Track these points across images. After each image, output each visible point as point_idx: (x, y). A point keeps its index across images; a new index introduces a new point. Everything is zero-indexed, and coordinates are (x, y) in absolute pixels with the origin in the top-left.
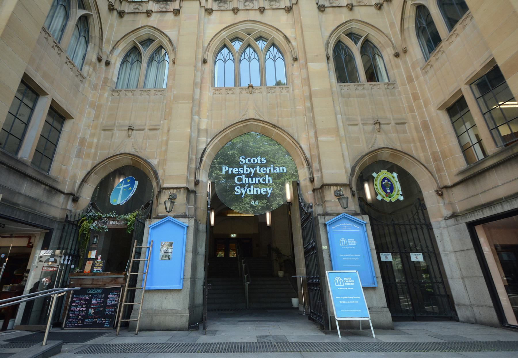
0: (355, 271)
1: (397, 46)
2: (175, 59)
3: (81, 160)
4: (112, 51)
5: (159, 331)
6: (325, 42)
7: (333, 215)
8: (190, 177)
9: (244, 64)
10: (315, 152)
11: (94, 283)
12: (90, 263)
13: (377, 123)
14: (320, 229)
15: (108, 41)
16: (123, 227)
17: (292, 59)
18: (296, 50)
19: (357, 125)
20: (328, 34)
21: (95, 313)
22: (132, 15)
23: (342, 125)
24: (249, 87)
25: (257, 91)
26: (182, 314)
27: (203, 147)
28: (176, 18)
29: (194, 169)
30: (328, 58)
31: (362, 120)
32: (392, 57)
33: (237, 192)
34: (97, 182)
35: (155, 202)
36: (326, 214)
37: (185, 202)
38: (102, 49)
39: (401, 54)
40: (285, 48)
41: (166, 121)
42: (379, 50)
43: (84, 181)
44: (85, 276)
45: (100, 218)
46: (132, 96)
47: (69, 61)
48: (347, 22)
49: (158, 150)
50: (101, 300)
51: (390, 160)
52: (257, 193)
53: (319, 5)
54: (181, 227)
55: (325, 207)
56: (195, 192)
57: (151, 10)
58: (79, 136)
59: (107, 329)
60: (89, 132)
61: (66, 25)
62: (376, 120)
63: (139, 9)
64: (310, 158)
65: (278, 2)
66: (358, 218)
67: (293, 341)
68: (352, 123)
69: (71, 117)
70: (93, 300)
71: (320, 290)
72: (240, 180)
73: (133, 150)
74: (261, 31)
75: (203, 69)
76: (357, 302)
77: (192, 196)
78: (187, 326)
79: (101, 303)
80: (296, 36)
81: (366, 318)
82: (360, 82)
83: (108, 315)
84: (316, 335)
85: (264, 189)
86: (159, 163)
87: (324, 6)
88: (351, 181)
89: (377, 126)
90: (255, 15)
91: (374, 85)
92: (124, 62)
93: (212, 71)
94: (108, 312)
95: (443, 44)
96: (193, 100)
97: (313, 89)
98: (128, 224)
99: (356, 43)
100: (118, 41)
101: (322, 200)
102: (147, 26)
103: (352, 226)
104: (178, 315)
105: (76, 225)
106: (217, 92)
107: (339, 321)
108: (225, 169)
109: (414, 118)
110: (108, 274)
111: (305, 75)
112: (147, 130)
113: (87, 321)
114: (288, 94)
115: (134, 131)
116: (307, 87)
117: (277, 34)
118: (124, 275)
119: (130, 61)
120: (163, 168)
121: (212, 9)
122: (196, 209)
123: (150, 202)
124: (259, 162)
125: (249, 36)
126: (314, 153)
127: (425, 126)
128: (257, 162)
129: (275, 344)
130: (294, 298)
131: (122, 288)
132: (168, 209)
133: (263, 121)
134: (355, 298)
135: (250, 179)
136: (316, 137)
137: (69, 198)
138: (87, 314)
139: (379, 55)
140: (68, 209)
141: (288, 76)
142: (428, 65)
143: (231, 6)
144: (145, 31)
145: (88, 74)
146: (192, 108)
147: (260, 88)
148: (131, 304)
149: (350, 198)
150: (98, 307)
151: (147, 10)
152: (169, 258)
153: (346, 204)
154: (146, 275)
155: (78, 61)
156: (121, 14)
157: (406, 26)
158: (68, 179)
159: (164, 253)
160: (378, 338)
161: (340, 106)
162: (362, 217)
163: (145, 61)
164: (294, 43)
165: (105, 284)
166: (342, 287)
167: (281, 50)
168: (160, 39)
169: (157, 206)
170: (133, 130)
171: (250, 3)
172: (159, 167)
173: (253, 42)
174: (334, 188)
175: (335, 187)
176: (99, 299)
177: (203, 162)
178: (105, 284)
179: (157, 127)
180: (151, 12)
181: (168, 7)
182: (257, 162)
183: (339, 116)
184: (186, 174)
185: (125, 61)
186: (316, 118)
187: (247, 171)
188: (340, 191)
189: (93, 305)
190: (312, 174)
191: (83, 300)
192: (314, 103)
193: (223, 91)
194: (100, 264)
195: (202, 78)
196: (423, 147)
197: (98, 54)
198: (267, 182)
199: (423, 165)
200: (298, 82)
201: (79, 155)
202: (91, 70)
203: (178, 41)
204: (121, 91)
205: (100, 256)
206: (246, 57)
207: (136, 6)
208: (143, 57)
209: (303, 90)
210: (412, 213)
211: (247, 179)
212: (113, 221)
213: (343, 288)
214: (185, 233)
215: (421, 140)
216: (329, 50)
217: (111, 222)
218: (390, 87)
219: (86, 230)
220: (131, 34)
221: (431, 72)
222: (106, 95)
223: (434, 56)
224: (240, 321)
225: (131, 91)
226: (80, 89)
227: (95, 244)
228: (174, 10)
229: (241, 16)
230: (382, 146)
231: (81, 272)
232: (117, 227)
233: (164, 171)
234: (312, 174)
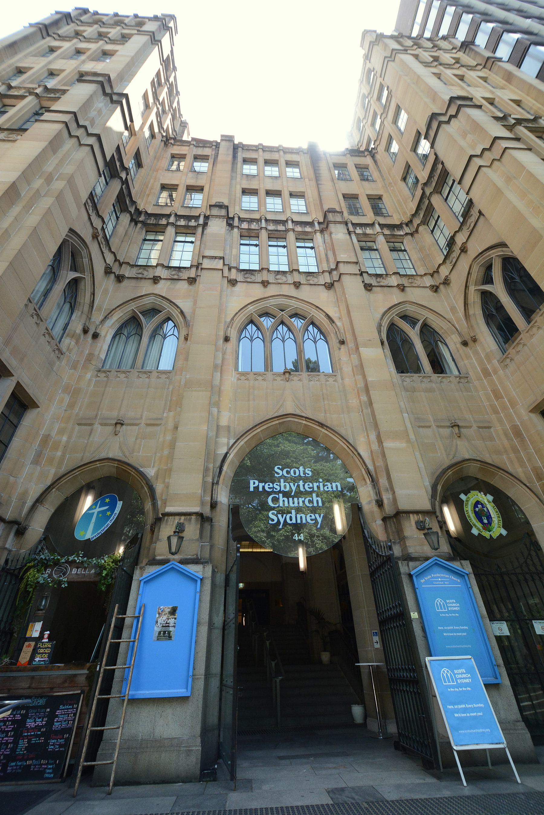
0: (470, 657)
1: (463, 333)
3: (39, 468)
4: (103, 321)
5: (150, 784)
7: (419, 560)
9: (277, 344)
10: (380, 463)
11: (33, 685)
12: (29, 646)
13: (455, 426)
14: (404, 583)
15: (100, 309)
16: (92, 580)
17: (338, 341)
18: (343, 331)
19: (429, 427)
20: (379, 316)
21: (31, 747)
22: (133, 281)
24: (284, 373)
26: (189, 747)
27: (224, 450)
28: (191, 287)
29: (211, 484)
30: (382, 343)
32: (459, 346)
33: (273, 520)
34: (58, 503)
35: (147, 536)
36: (408, 558)
38: (90, 319)
39: (470, 343)
41: (172, 414)
42: (441, 337)
43: (39, 500)
44: (20, 671)
45: (56, 563)
46: (126, 379)
47: (48, 333)
48: (399, 303)
49: (158, 455)
50: (43, 721)
51: (479, 476)
52: (301, 521)
54: (192, 579)
55: (406, 546)
58: (42, 432)
59: (50, 783)
60: (56, 427)
61: (51, 288)
62: (453, 421)
65: (315, 277)
66: (456, 565)
67: (393, 798)
68: (423, 424)
69: (35, 405)
70: (28, 720)
71: (419, 694)
72: (275, 500)
73: (120, 454)
75: (225, 348)
76: (481, 714)
77: (207, 526)
78: (198, 772)
79: (42, 726)
81: (500, 743)
82: (425, 373)
83: (53, 751)
84: (421, 781)
85: (311, 516)
86: (157, 476)
87: (371, 285)
89: (456, 429)
90: (290, 291)
91: (443, 377)
92: (116, 335)
94: (54, 744)
95: (523, 336)
97: (370, 379)
98: (104, 575)
100: (113, 310)
101: (398, 535)
103: (449, 578)
104: (182, 749)
105: (17, 576)
106: (243, 378)
107: (458, 752)
108: (254, 483)
109: (500, 420)
110: (59, 667)
111: (356, 362)
112: (143, 425)
113: (12, 766)
114: (336, 384)
115: (124, 427)
118: (88, 670)
119: (126, 333)
121: (236, 280)
122: (212, 547)
123: (139, 536)
124: (302, 475)
127: (518, 433)
129: (366, 805)
130: (355, 704)
131: (82, 696)
132: (173, 550)
133: (306, 418)
134: (477, 705)
137: (11, 529)
138: (14, 750)
139: (441, 342)
140: (6, 548)
142: (507, 358)
143: (259, 278)
144: (149, 300)
145: (68, 349)
147: (108, 371)
148: (99, 728)
150: (36, 736)
152: (170, 637)
154: (131, 670)
155: (57, 331)
156: (120, 279)
157: (471, 312)
158: (14, 499)
159: (163, 626)
160: (526, 784)
162: (461, 564)
163: (146, 334)
164: (339, 324)
165: (52, 688)
166: (453, 687)
167: (323, 331)
169: (151, 542)
170: (122, 424)
172: (157, 479)
173: (287, 320)
174: (414, 517)
175: (415, 515)
176: (39, 718)
177: (223, 473)
178: (52, 688)
179: (158, 422)
181: (180, 274)
183: (405, 415)
185: (118, 334)
186: (377, 417)
189: (28, 730)
190: (378, 493)
191: (10, 721)
193: (251, 376)
194: (46, 648)
196: (520, 460)
197: (85, 324)
198: (315, 504)
199: (525, 485)
200: (347, 369)
201: (36, 461)
202: (73, 343)
204: (110, 371)
205: (48, 632)
206: (279, 336)
207: (140, 271)
208: (144, 330)
209: (355, 380)
210: (523, 556)
211: (286, 499)
212: (78, 568)
213: (456, 689)
214: (198, 590)
215: (515, 451)
216: (382, 334)
217: (74, 571)
218: (462, 380)
219: (31, 585)
220: (131, 302)
221: (512, 366)
222: (89, 376)
223: (513, 348)
224: (281, 758)
225: (124, 372)
226: (55, 369)
227: (42, 610)
228: (189, 278)
229: (272, 290)
230: (467, 456)
231: (12, 664)
232: (83, 580)
233: (167, 487)
234: (378, 493)
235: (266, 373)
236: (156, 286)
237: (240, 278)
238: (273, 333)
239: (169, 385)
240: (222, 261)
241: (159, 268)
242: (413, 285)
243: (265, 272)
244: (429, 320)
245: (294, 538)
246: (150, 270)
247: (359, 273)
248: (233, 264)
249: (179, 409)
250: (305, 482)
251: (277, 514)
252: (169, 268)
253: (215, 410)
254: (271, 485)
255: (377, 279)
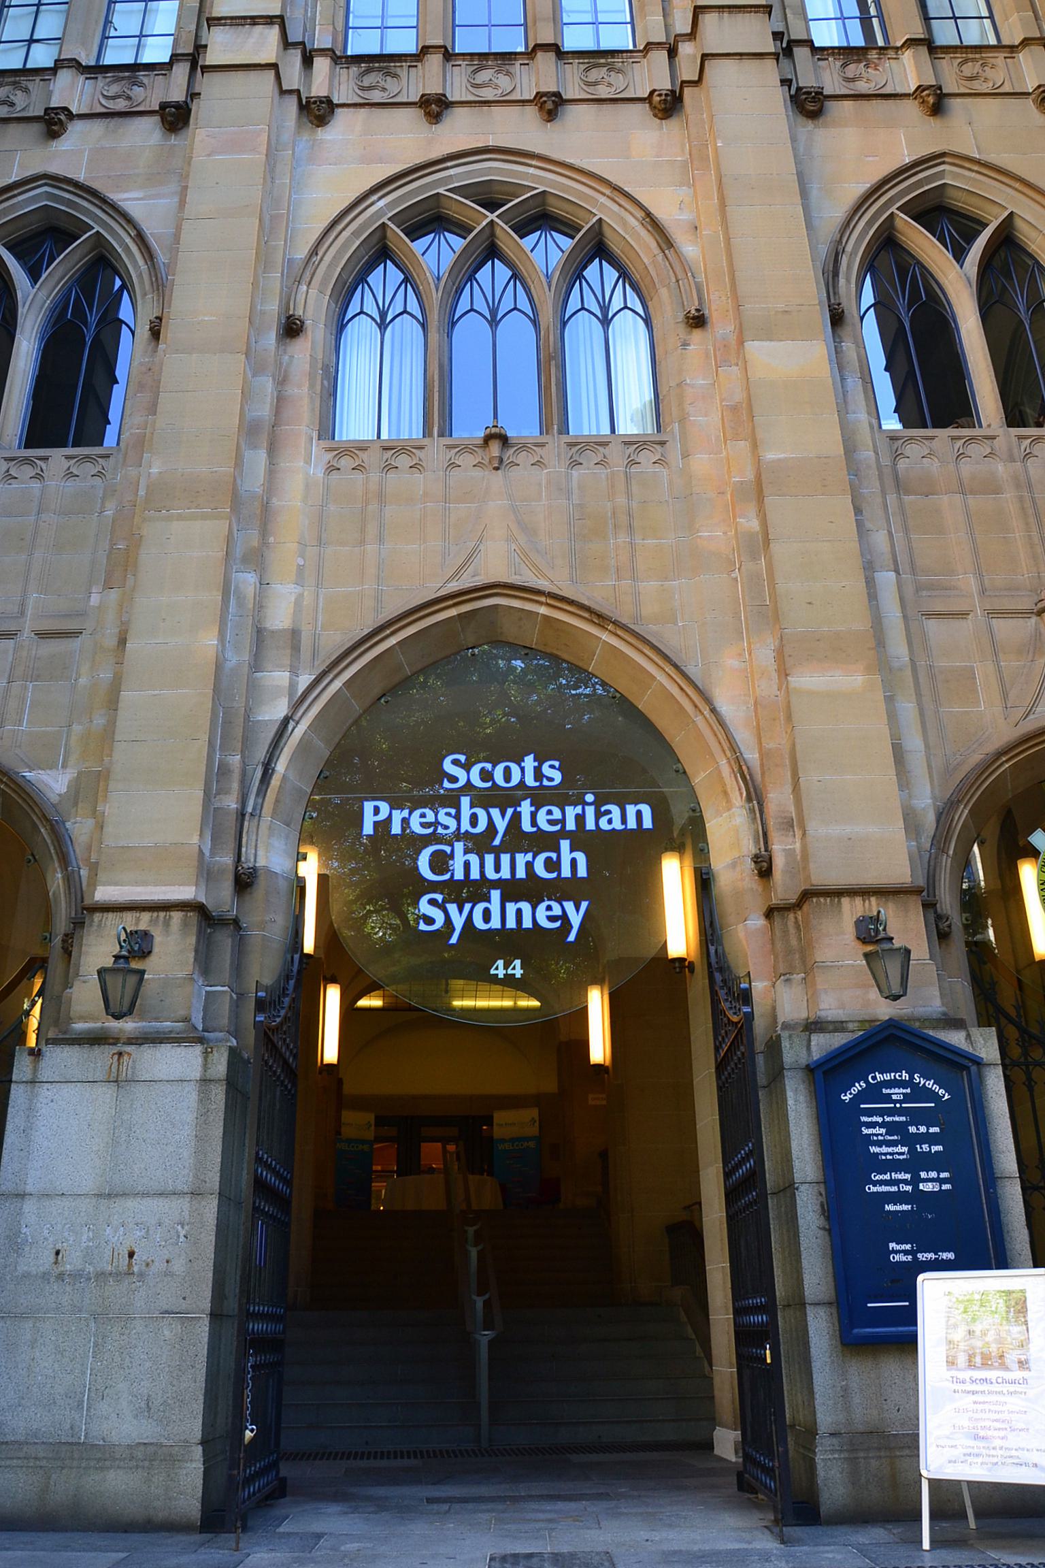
2: (160, 319)
6: (824, 249)
8: (213, 854)
9: (471, 331)
17: (681, 316)
19: (963, 615)
23: (899, 614)
24: (488, 439)
25: (522, 458)
27: (280, 709)
28: (174, 141)
31: (983, 591)
37: (191, 968)
40: (650, 268)
41: (114, 595)
49: (77, 728)
53: (799, 89)
56: (236, 922)
57: (65, 109)
63: (12, 104)
64: (758, 763)
65: (619, 71)
72: (440, 862)
74: (544, 192)
80: (698, 216)
82: (981, 426)
86: (76, 793)
87: (819, 93)
88: (931, 878)
93: (326, 368)
96: (236, 501)
99: (959, 255)
102: (45, 176)
108: (377, 811)
114: (665, 472)
116: (743, 446)
117: (615, 208)
120: (94, 811)
125: (492, 216)
126: (772, 745)
128: (522, 782)
135: (489, 859)
136: (784, 673)
141: (663, 391)
146: (229, 539)
147: (537, 445)
149: (920, 950)
151: (47, 109)
153: (899, 980)
161: (890, 533)
163: (28, 324)
164: (690, 249)
168: (98, 231)
171: (498, 72)
172: (76, 804)
173: (506, 235)
175: (858, 901)
177: (275, 782)
180: (62, 117)
181: (137, 92)
182: (522, 782)
184: (195, 840)
187: (474, 820)
188: (876, 919)
192: (771, 517)
193: (372, 458)
195: (280, 401)
198: (566, 872)
203: (177, 237)
206: (480, 305)
211: (474, 859)
216: (842, 281)
224: (430, 1501)
233: (101, 827)
235: (426, 441)
236: (54, 143)
237: (345, 88)
238: (460, 292)
239: (103, 499)
240: (275, 31)
241: (65, 76)
242: (980, 87)
243: (435, 60)
244: (1019, 223)
245: (492, 972)
246: (35, 85)
247: (770, 47)
248: (322, 40)
249: (130, 581)
250: (537, 804)
251: (444, 901)
252: (97, 70)
253: (248, 580)
254: (430, 817)
255: (844, 65)
